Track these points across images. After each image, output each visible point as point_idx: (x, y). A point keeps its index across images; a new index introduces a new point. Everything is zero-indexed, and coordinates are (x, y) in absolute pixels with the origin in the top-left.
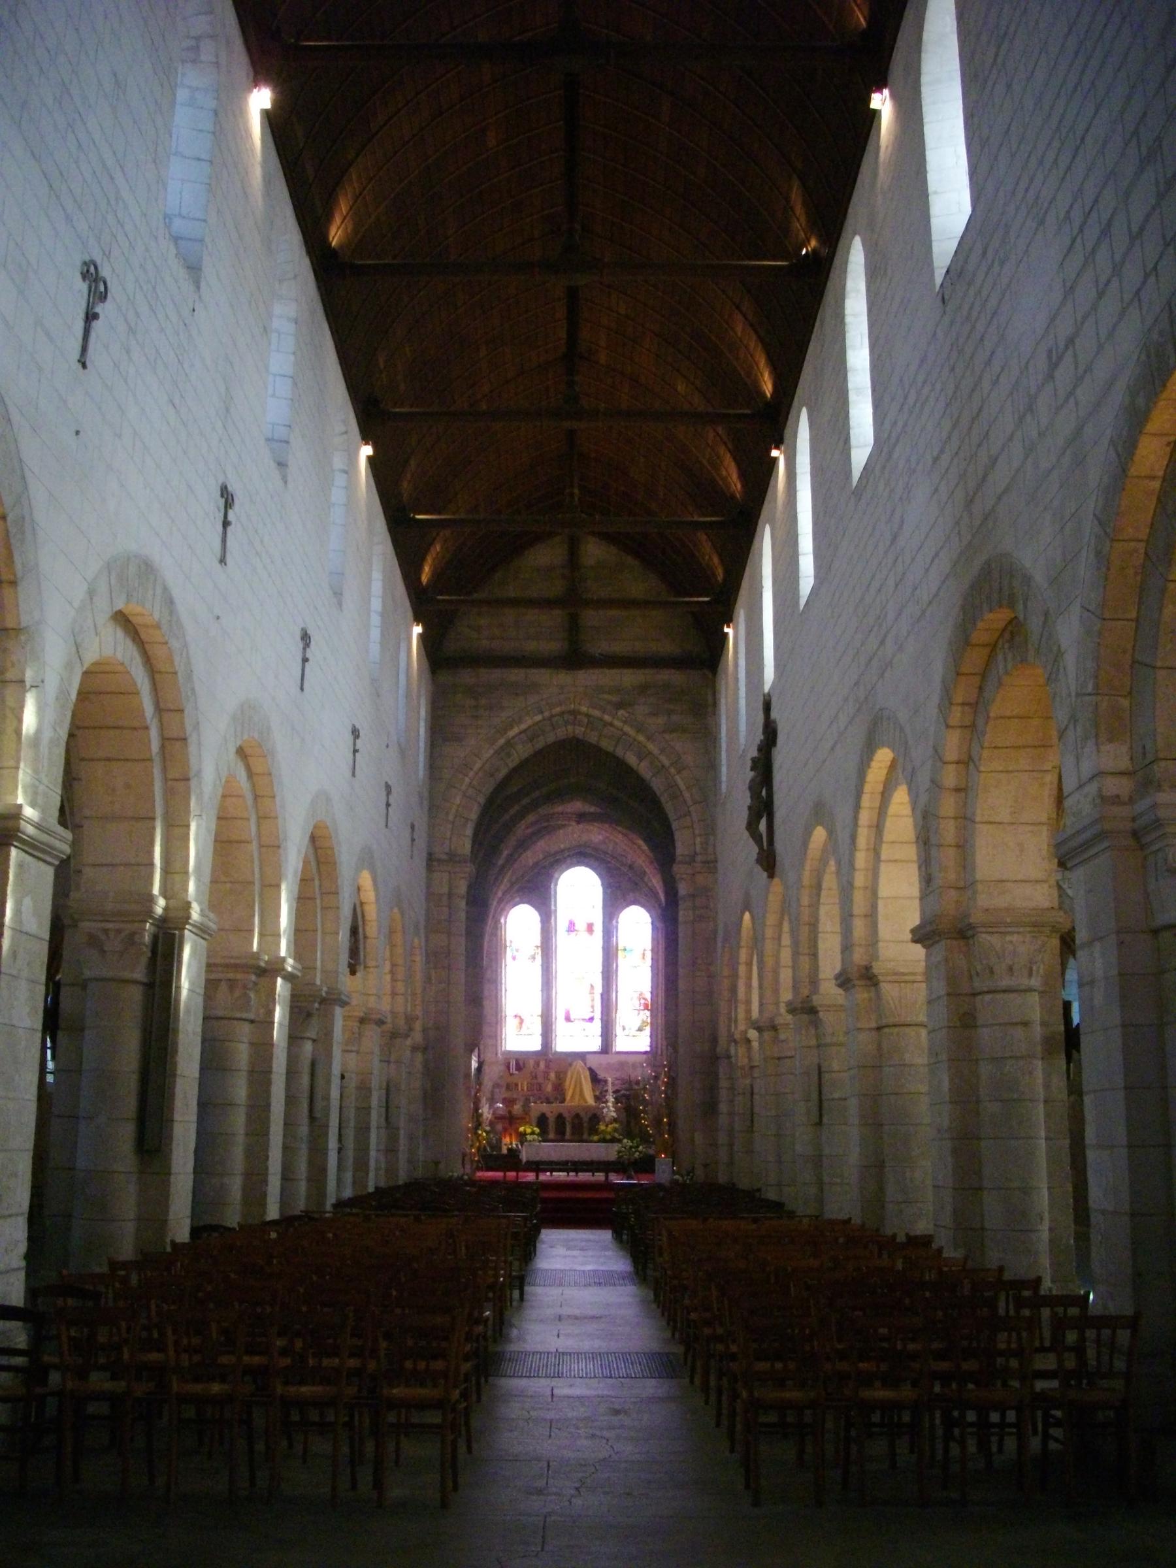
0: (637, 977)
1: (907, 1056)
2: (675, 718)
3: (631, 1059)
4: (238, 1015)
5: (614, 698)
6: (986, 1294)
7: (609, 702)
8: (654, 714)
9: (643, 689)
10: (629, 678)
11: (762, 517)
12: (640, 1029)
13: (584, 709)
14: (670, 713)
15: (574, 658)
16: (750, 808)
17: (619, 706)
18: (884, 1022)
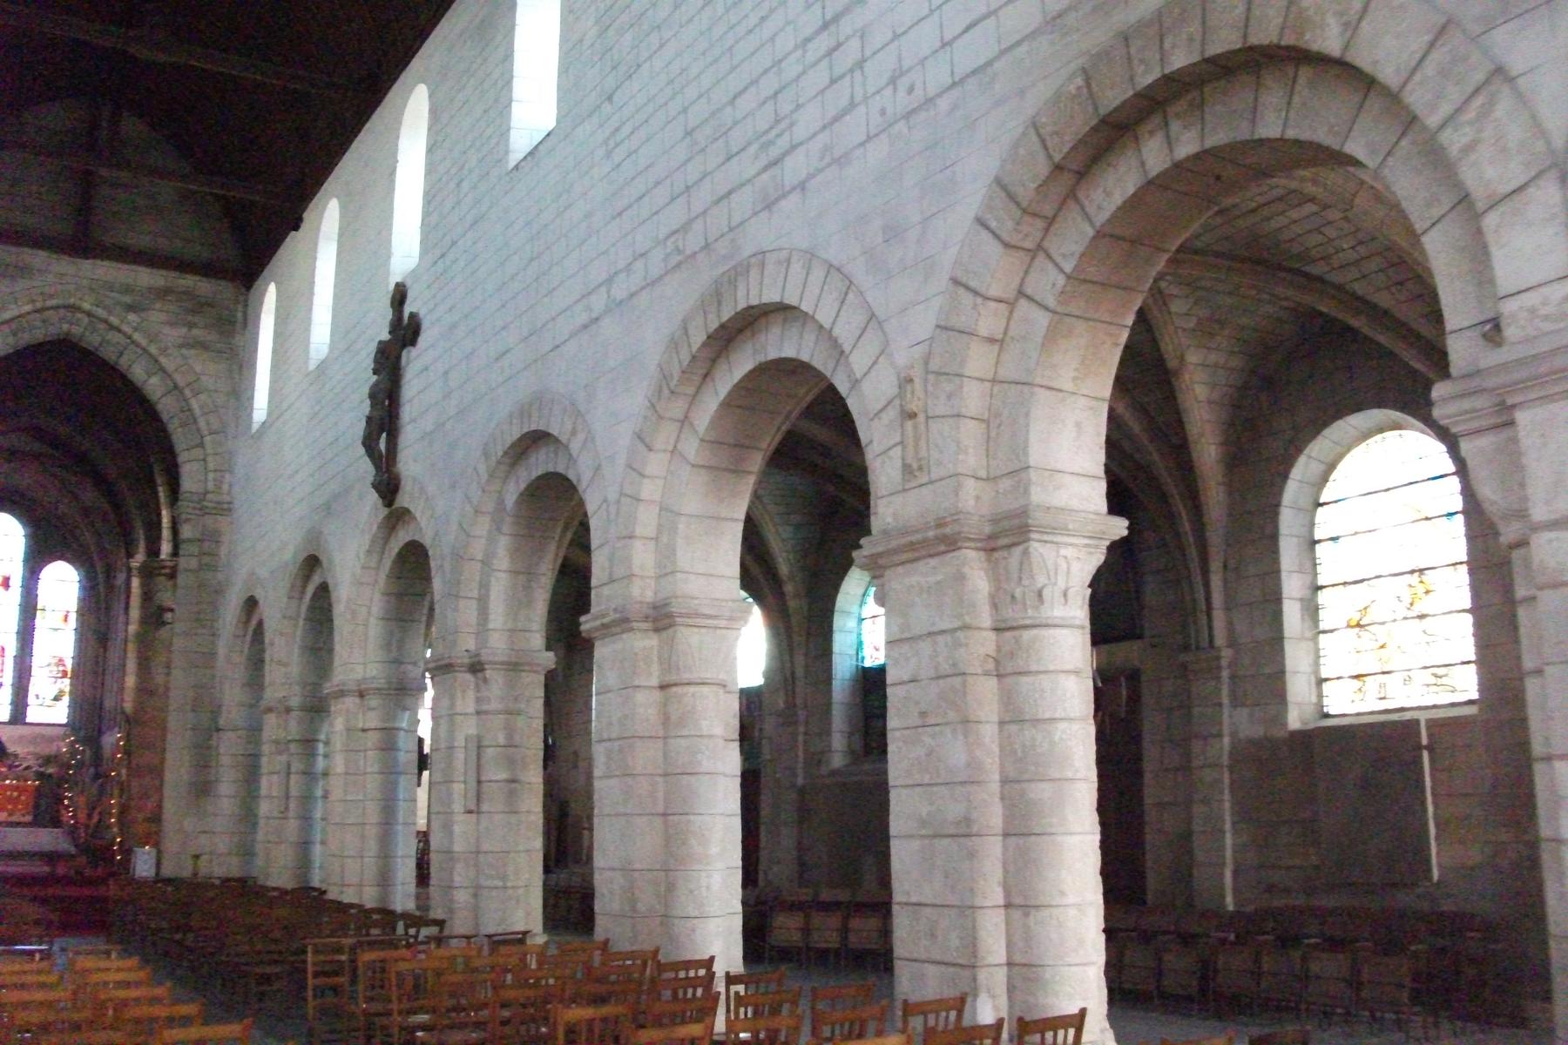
0: (58, 640)
1: (704, 724)
2: (195, 332)
3: (49, 731)
4: (1435, 56)
5: (127, 299)
6: (742, 1035)
7: (118, 303)
8: (171, 324)
9: (163, 293)
10: (145, 277)
11: (417, 64)
12: (57, 699)
13: (86, 306)
14: (191, 326)
15: (81, 244)
16: (369, 420)
17: (131, 308)
18: (673, 678)
